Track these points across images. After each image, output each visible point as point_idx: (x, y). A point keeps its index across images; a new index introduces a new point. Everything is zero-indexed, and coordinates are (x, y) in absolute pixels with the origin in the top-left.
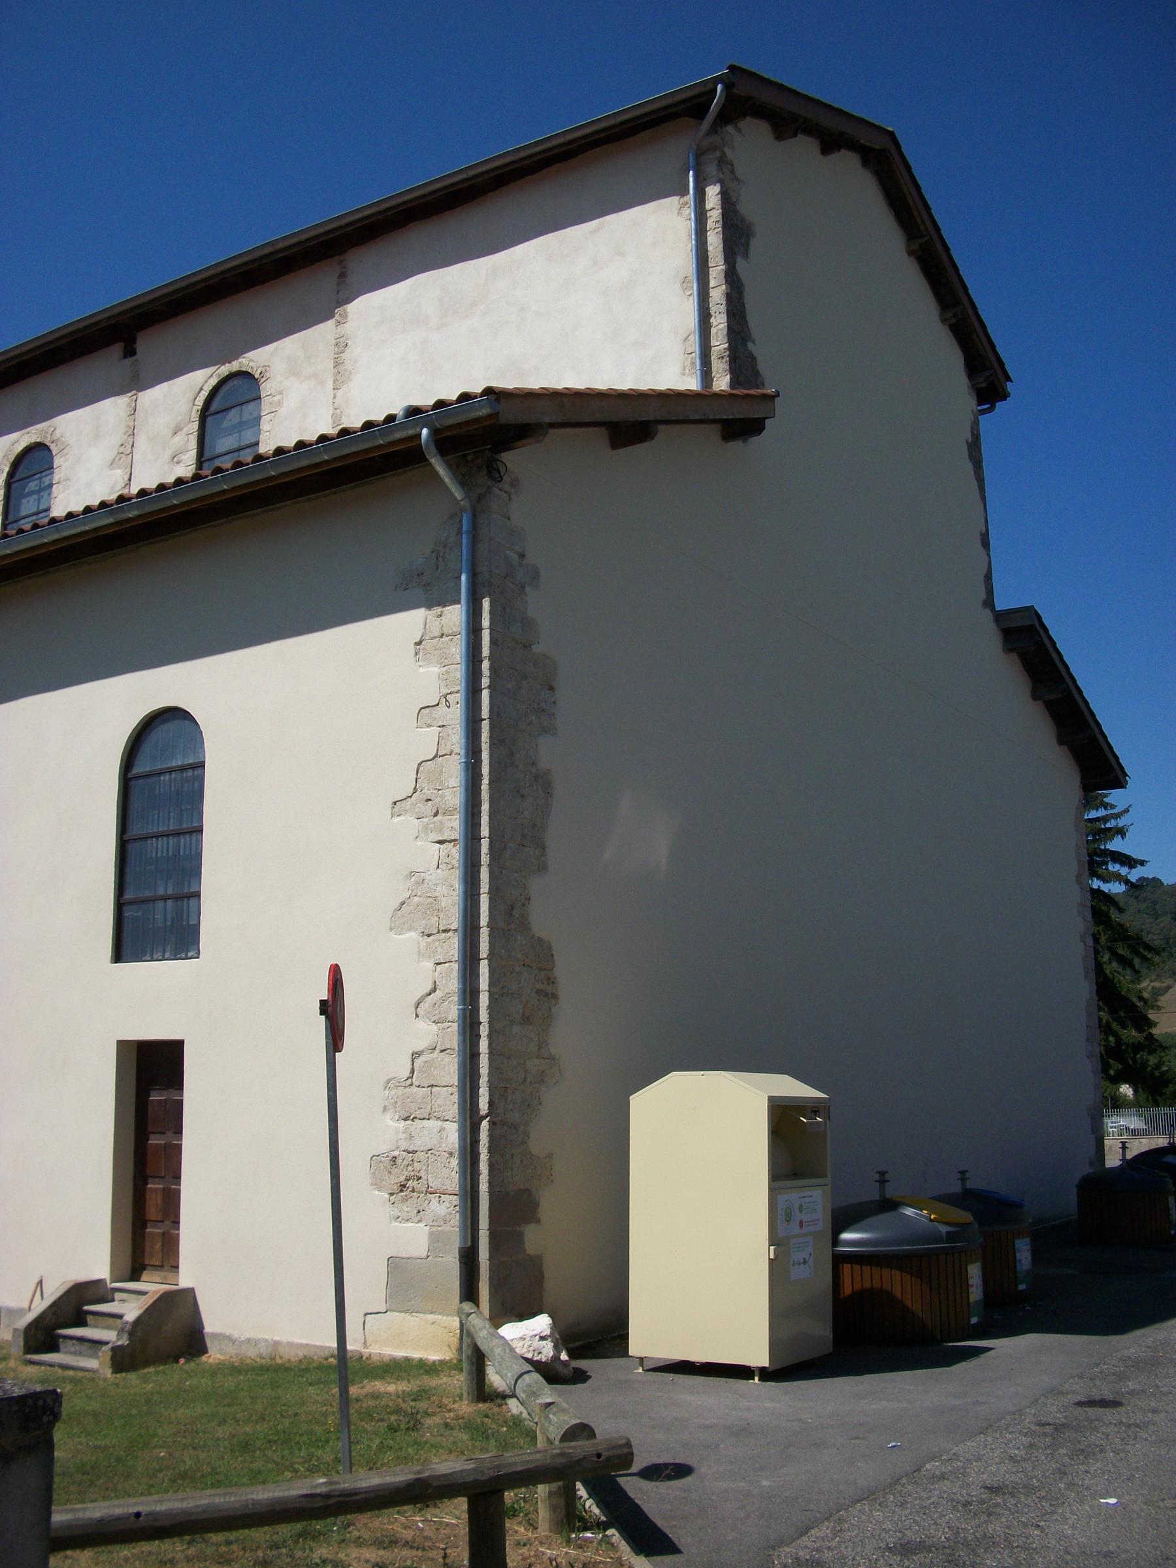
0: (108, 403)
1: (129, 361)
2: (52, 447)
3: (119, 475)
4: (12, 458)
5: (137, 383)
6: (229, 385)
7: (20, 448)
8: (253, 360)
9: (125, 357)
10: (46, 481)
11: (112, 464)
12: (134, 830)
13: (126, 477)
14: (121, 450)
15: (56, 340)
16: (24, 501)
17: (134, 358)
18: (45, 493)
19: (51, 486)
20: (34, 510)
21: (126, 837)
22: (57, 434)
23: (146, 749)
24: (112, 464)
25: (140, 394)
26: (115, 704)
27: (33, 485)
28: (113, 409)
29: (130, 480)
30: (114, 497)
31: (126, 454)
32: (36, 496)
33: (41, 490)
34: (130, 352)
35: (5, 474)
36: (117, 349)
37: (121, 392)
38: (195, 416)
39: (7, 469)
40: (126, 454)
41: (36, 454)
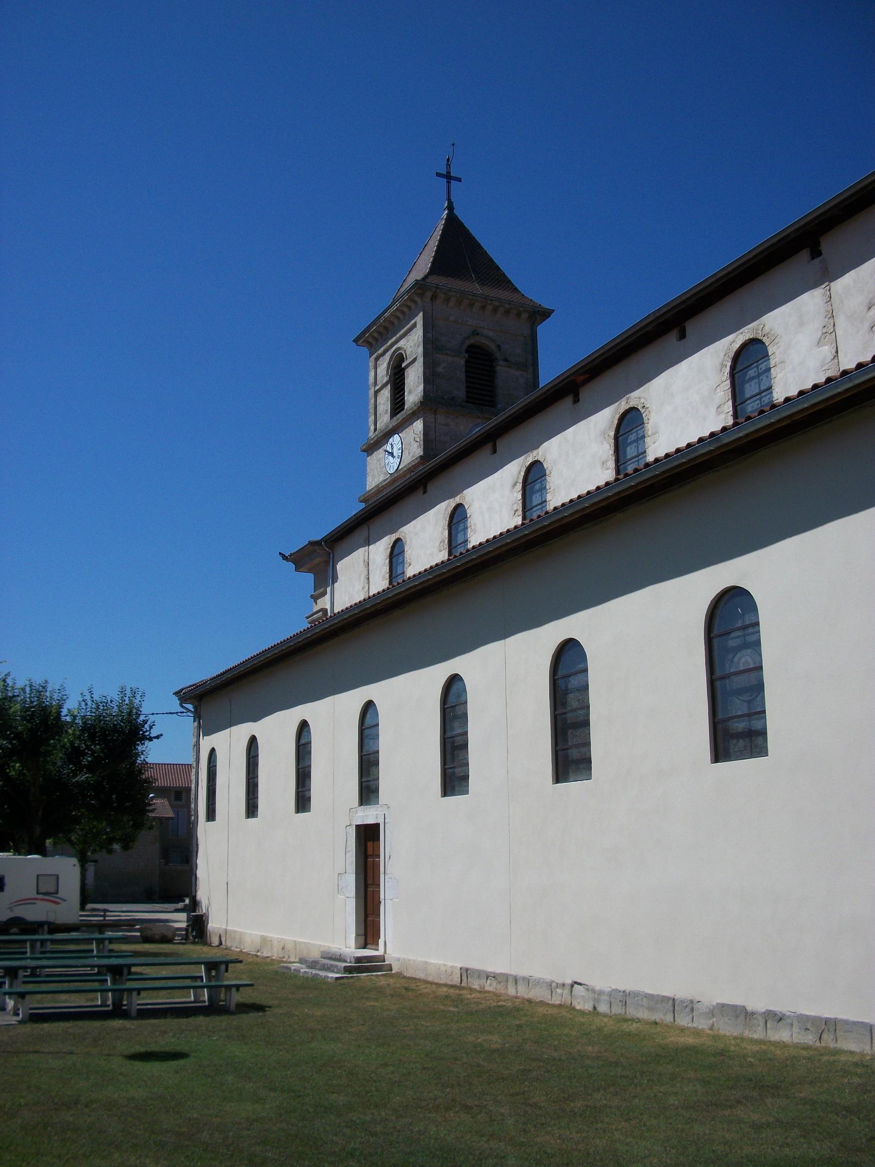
0: (806, 297)
1: (817, 261)
2: (764, 340)
3: (827, 350)
4: (732, 354)
5: (828, 276)
6: (628, 417)
7: (737, 346)
8: (635, 398)
9: (813, 258)
10: (763, 367)
11: (819, 343)
12: (718, 673)
13: (834, 351)
14: (825, 330)
15: (755, 257)
16: (747, 386)
17: (821, 258)
18: (764, 377)
19: (768, 370)
20: (757, 391)
21: (714, 677)
22: (767, 329)
23: (717, 621)
24: (819, 343)
25: (832, 284)
26: (703, 585)
27: (632, 437)
28: (811, 301)
29: (837, 352)
30: (603, 483)
31: (829, 332)
32: (756, 380)
33: (759, 376)
34: (816, 253)
35: (728, 368)
36: (805, 254)
37: (815, 285)
38: (446, 527)
39: (729, 364)
40: (829, 332)
41: (399, 543)
